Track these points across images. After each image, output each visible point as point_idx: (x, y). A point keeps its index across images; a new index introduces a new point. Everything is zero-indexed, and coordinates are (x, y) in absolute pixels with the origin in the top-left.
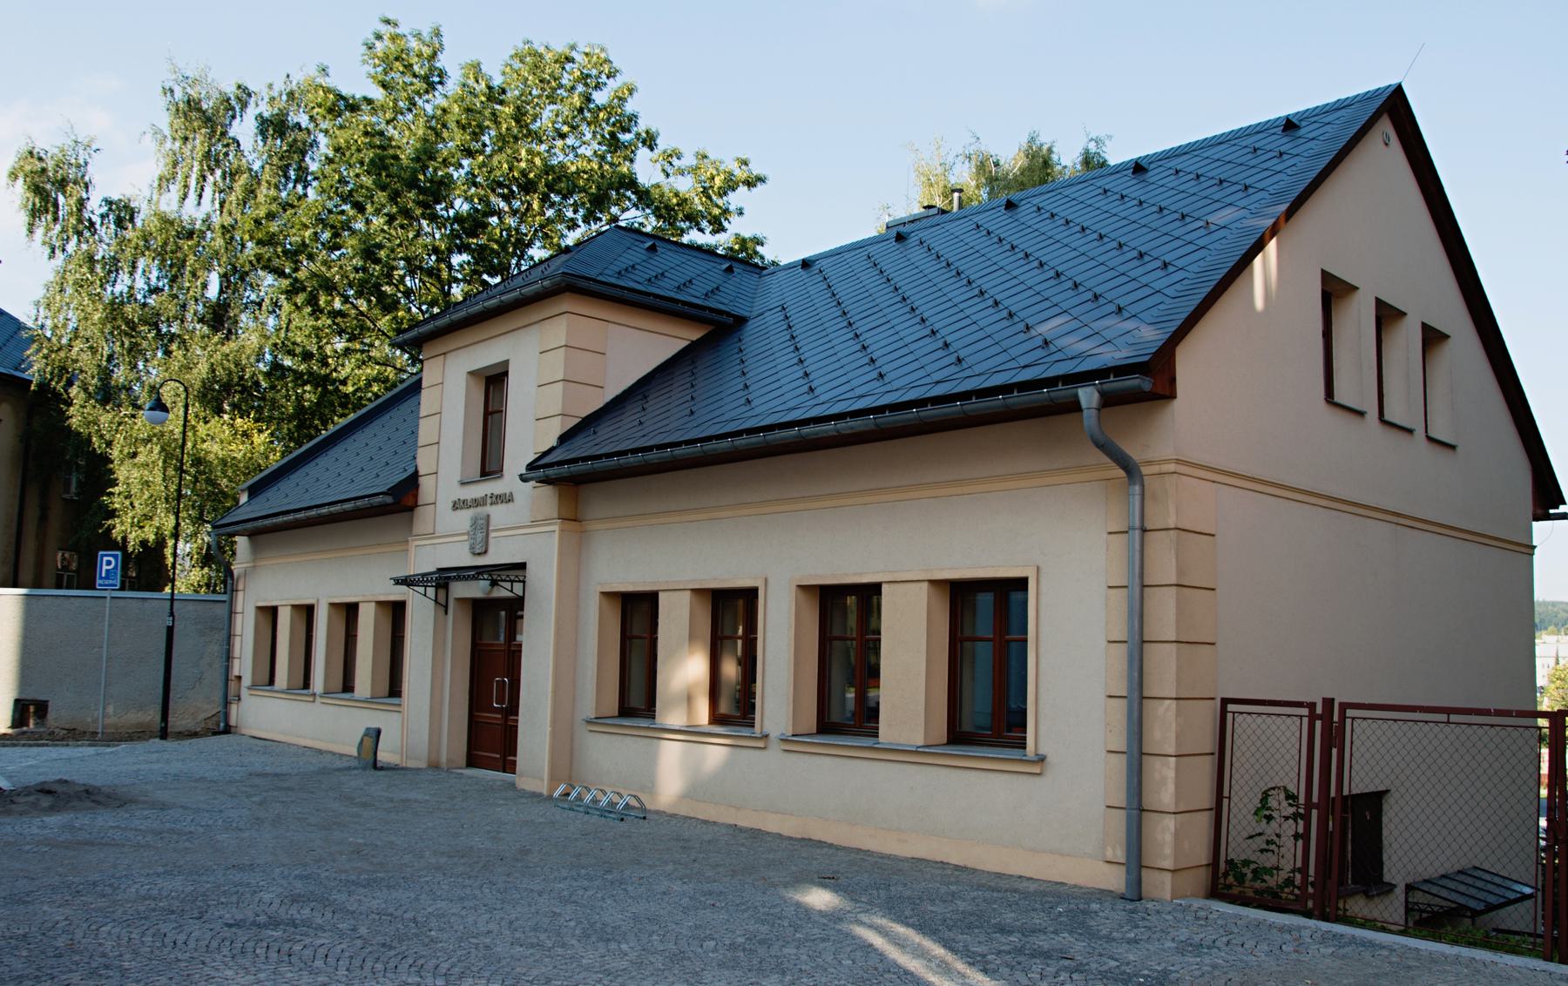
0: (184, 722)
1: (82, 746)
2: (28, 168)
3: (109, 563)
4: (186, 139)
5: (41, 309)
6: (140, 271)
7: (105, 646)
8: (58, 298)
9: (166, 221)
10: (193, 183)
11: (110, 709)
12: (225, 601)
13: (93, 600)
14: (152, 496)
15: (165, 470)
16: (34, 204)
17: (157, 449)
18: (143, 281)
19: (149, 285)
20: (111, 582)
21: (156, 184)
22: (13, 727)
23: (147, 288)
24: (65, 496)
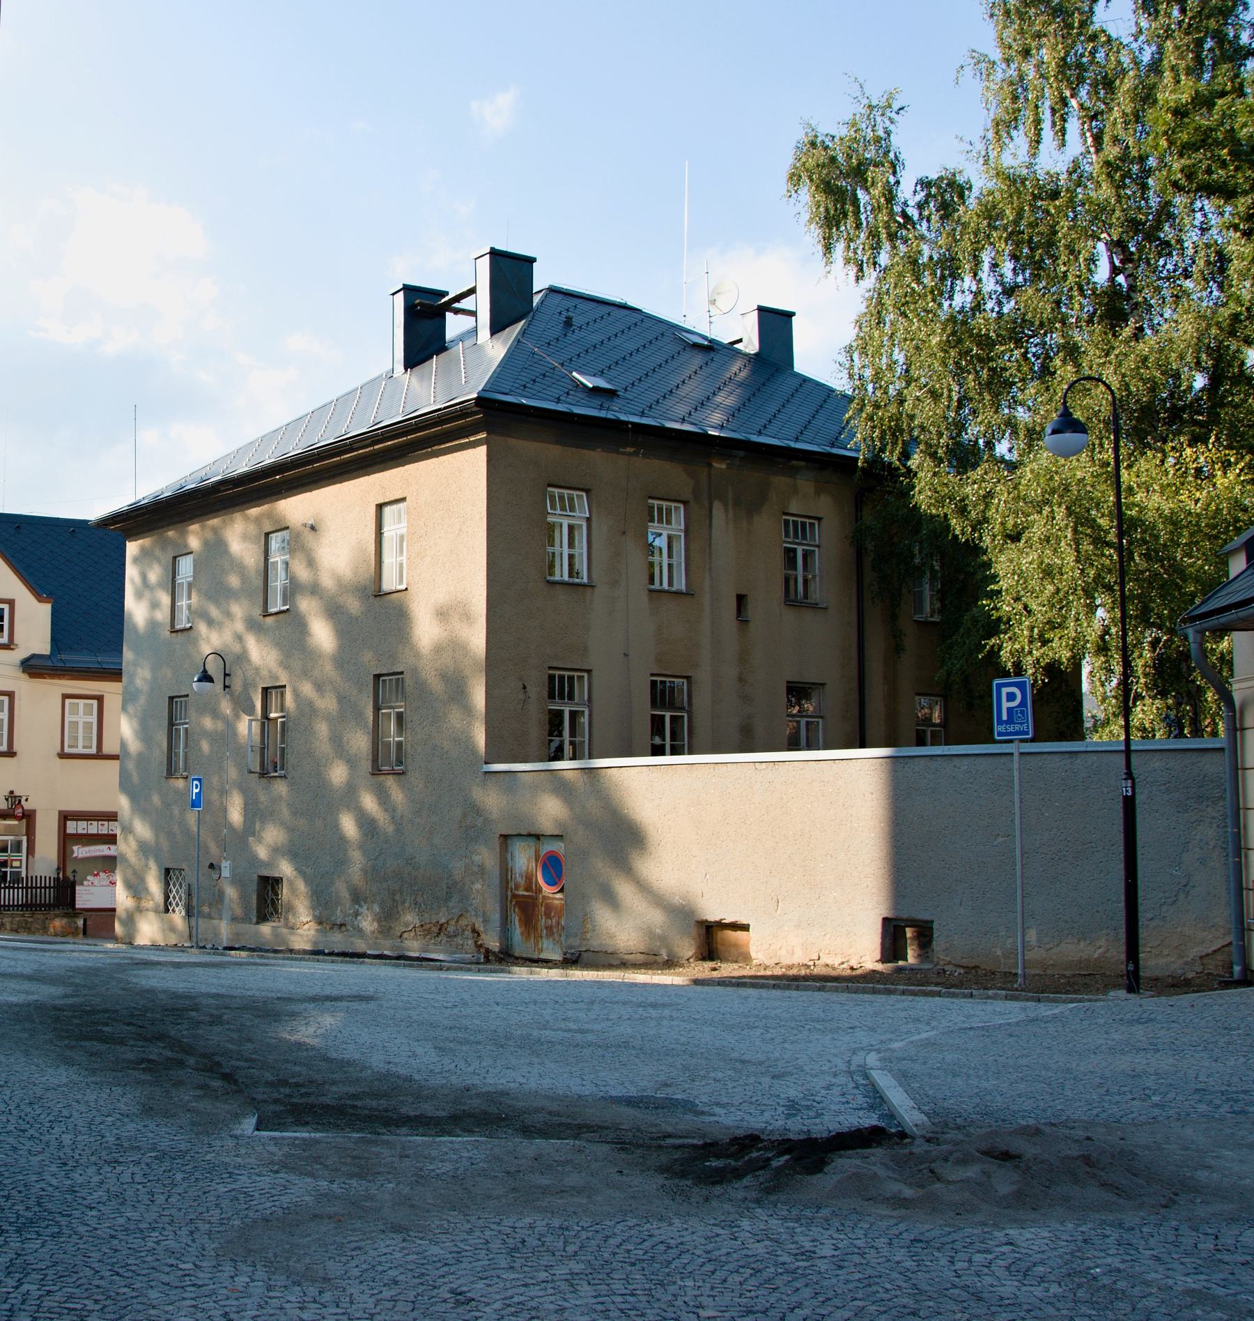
0: (1162, 961)
1: (995, 997)
2: (811, 163)
3: (1011, 697)
4: (1026, 53)
5: (856, 356)
6: (986, 266)
7: (1018, 833)
8: (876, 334)
9: (1013, 181)
10: (1046, 116)
11: (1032, 936)
12: (1222, 750)
13: (990, 759)
14: (1058, 590)
15: (1077, 544)
16: (827, 210)
17: (1060, 513)
18: (992, 280)
19: (1002, 284)
20: (1017, 727)
21: (990, 135)
22: (884, 959)
23: (1000, 289)
24: (917, 617)
